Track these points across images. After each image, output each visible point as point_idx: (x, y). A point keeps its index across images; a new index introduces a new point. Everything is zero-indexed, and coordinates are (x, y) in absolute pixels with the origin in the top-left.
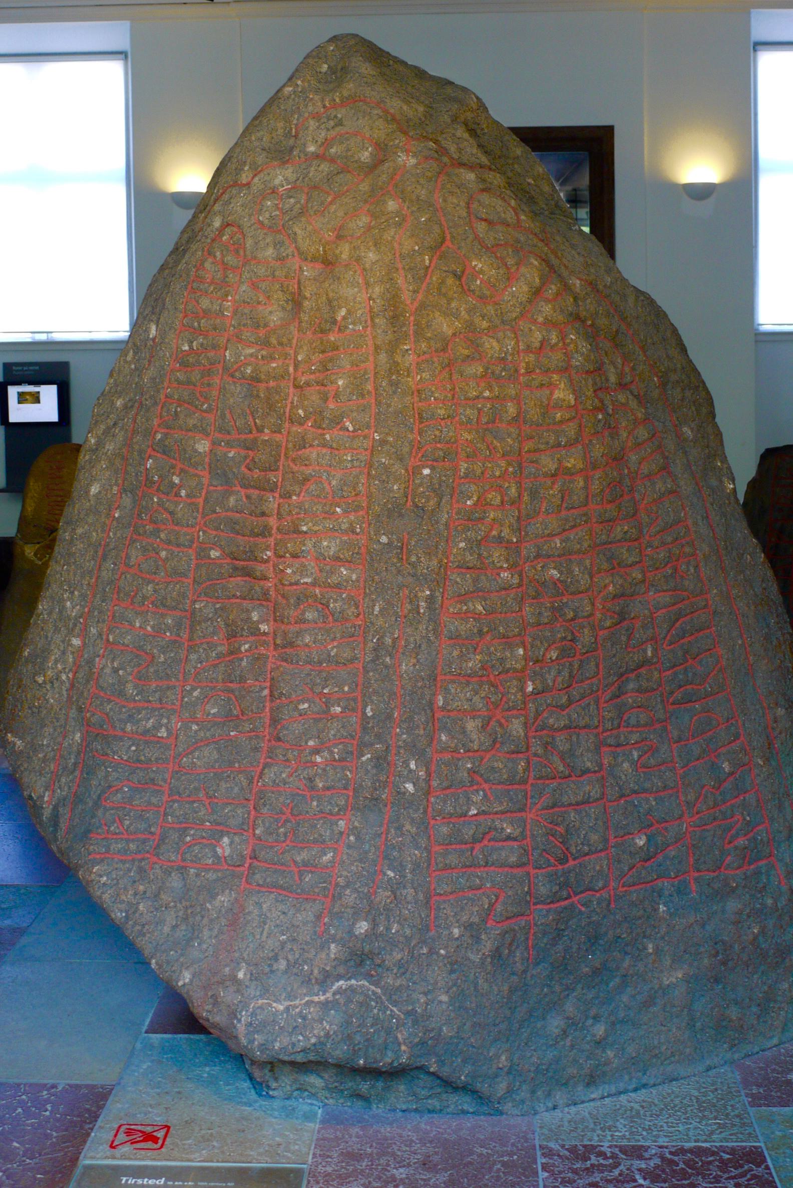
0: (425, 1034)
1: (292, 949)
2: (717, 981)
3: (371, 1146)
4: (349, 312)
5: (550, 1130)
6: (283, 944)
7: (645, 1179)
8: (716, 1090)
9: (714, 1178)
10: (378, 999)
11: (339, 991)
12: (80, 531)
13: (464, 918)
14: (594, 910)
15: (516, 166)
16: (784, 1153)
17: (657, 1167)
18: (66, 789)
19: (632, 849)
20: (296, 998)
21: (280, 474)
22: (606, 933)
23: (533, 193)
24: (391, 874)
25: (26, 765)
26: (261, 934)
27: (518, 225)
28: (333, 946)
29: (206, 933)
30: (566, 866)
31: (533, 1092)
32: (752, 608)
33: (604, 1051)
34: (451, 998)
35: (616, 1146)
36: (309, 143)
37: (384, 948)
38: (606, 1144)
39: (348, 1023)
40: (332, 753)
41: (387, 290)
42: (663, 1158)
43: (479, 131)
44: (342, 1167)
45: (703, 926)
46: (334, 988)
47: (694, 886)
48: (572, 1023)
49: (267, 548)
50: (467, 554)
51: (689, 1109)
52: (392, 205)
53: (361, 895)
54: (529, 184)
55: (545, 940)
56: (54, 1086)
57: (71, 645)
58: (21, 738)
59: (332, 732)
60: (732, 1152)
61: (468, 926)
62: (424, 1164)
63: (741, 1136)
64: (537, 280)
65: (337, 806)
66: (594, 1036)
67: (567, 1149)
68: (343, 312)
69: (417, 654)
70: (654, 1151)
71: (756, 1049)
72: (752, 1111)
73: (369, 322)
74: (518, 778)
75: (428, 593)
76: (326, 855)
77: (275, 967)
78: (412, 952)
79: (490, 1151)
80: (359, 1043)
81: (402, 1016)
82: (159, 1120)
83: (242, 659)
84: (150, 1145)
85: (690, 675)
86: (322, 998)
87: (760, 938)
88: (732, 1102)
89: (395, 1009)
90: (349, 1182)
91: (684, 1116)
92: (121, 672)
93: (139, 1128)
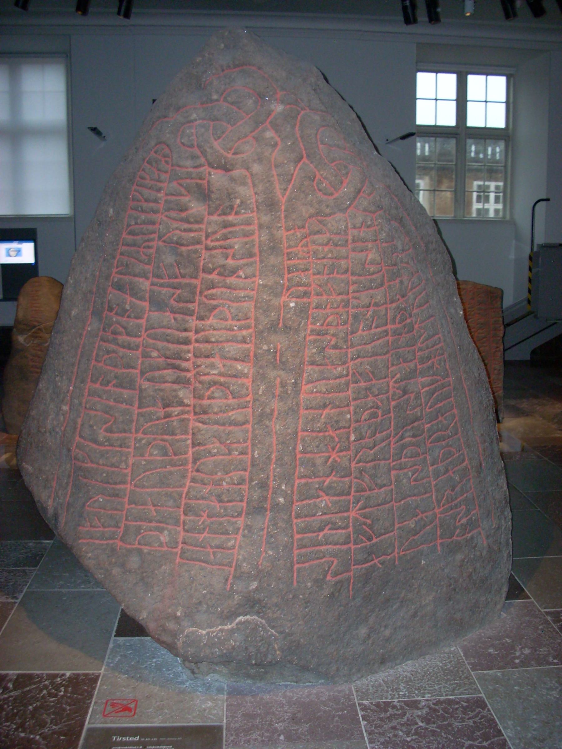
2: (450, 599)
4: (242, 202)
6: (204, 596)
7: (423, 722)
8: (451, 661)
9: (461, 719)
10: (263, 627)
11: (240, 623)
12: (65, 339)
16: (496, 700)
17: (427, 714)
18: (62, 498)
21: (196, 304)
24: (270, 553)
26: (191, 589)
35: (402, 701)
38: (396, 700)
40: (232, 479)
42: (430, 708)
44: (245, 724)
49: (189, 352)
51: (439, 674)
52: (269, 134)
55: (359, 585)
59: (233, 467)
60: (468, 701)
61: (316, 581)
62: (293, 719)
63: (471, 691)
65: (237, 512)
66: (385, 636)
67: (374, 705)
68: (238, 201)
70: (424, 703)
73: (255, 209)
74: (345, 492)
75: (294, 381)
77: (200, 609)
79: (330, 709)
81: (277, 635)
82: (131, 696)
84: (127, 713)
85: (440, 426)
86: (230, 627)
87: (473, 574)
89: (273, 631)
90: (251, 734)
93: (119, 702)
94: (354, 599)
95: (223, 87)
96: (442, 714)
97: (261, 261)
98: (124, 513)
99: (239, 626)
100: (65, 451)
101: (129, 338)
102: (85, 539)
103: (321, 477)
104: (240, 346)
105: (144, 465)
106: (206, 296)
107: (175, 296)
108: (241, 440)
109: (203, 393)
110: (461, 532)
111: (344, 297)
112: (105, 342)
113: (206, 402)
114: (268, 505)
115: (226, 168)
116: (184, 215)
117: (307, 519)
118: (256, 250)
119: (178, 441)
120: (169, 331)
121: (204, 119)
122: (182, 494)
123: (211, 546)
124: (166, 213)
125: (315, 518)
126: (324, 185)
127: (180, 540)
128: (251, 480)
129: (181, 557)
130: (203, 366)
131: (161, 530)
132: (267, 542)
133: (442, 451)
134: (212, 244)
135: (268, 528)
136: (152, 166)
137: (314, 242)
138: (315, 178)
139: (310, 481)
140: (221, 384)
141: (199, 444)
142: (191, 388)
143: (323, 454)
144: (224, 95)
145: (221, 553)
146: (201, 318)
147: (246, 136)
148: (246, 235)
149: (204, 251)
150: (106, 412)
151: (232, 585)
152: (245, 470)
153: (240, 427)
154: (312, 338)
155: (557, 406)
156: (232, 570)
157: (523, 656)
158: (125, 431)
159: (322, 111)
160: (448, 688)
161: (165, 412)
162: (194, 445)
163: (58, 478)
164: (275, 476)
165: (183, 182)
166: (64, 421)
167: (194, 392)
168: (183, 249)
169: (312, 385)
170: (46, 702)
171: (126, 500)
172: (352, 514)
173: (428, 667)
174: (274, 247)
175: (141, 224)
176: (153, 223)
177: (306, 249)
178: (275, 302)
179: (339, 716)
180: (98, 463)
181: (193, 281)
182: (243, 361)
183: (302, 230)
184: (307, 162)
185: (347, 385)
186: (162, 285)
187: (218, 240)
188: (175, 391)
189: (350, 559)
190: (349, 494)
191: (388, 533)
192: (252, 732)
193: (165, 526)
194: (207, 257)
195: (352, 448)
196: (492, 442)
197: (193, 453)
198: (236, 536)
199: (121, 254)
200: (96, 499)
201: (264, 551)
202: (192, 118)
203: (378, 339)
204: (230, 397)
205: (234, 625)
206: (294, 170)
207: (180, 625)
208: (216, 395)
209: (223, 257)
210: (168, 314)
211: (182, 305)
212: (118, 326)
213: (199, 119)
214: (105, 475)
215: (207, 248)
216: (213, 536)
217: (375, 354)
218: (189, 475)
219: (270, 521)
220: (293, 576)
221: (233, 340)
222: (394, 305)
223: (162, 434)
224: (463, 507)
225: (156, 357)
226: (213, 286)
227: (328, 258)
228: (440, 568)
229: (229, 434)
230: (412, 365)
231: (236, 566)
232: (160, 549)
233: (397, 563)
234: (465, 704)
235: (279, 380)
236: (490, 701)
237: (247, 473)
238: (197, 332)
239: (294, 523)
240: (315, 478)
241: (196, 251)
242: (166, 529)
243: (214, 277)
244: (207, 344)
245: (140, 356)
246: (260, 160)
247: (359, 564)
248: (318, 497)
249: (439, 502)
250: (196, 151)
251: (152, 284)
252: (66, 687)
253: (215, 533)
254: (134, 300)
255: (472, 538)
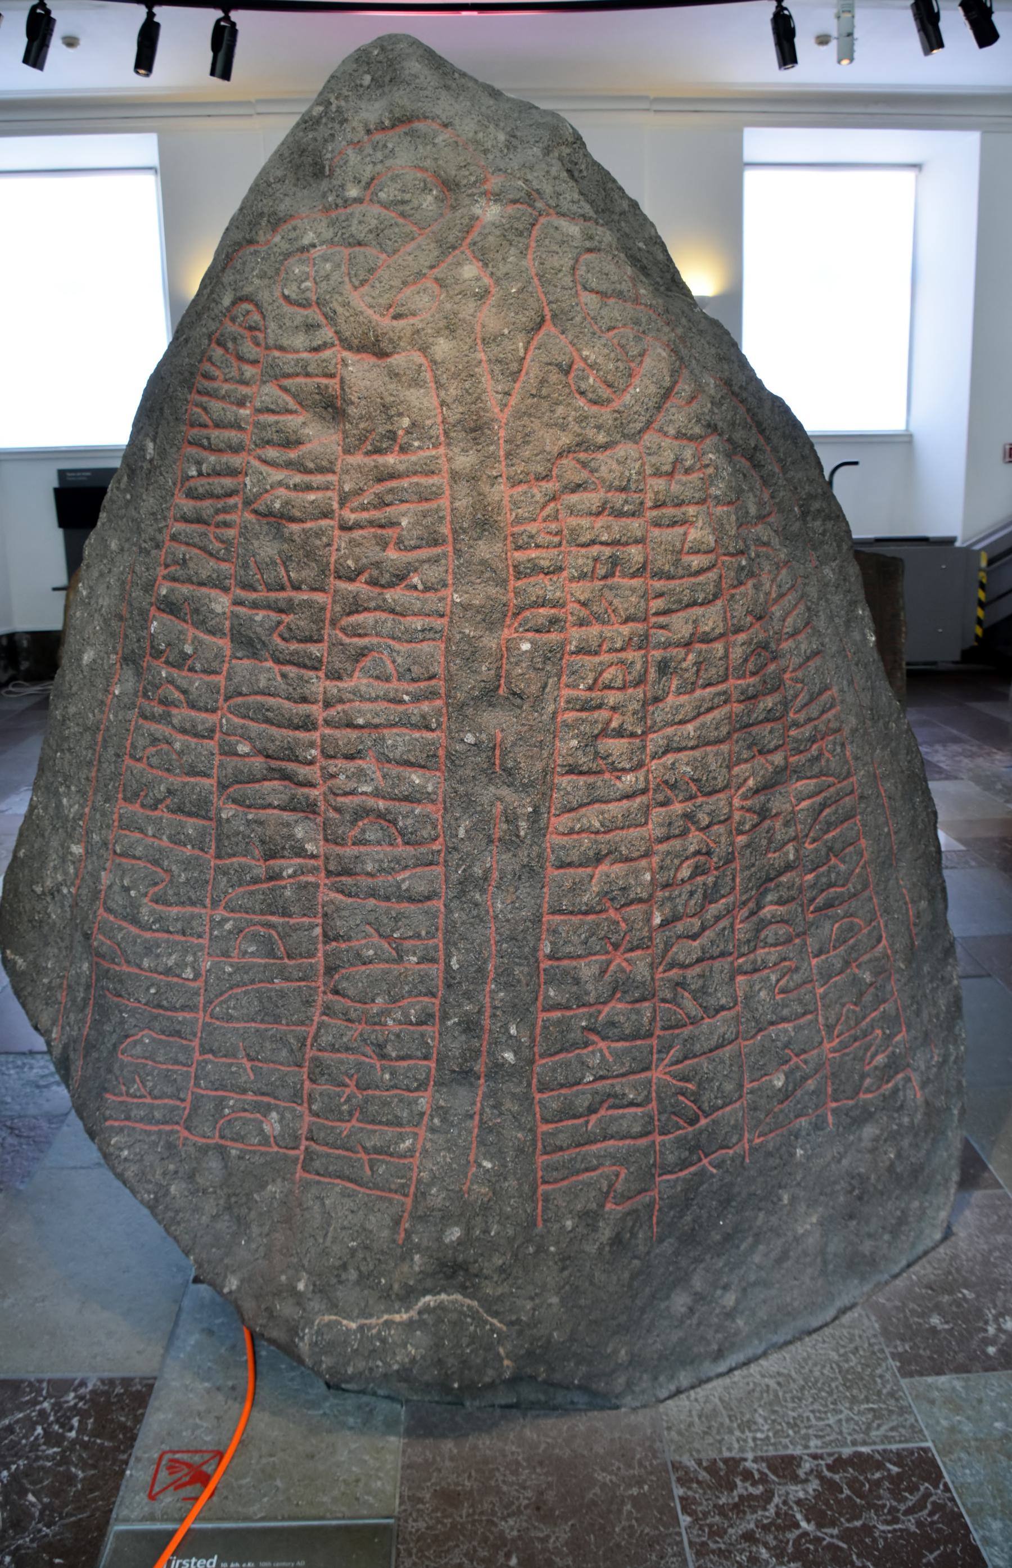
0: (532, 1344)
1: (365, 1259)
2: (851, 1217)
3: (470, 1477)
4: (413, 424)
5: (680, 1433)
6: (353, 1252)
7: (808, 1521)
8: (856, 1349)
10: (475, 1315)
11: (426, 1309)
12: (72, 710)
13: (579, 1207)
14: (727, 1171)
15: (623, 224)
16: (960, 1459)
17: (818, 1496)
19: (769, 1092)
20: (371, 1316)
22: (739, 1193)
23: (645, 261)
24: (488, 1165)
25: (29, 989)
26: (325, 1236)
27: (636, 300)
28: (417, 1257)
29: (255, 1230)
30: (697, 1126)
31: (655, 1378)
32: (900, 787)
33: (734, 1321)
34: (563, 1300)
36: (349, 185)
37: (482, 1255)
38: (750, 1456)
39: (438, 1346)
40: (406, 1015)
41: (467, 391)
43: (576, 174)
44: (439, 1521)
45: (839, 1161)
46: (420, 1304)
47: (830, 1119)
48: (699, 1298)
49: (312, 745)
50: (580, 753)
51: (833, 1385)
52: (470, 271)
53: (452, 1194)
54: (640, 249)
55: (672, 1213)
56: (83, 1383)
57: (71, 853)
58: (22, 955)
59: (407, 988)
63: (903, 1431)
64: (667, 378)
65: (416, 1080)
68: (406, 422)
69: (517, 889)
71: (886, 1276)
72: (904, 1382)
73: (442, 439)
75: (530, 809)
76: (404, 1142)
77: (344, 1277)
78: (515, 1256)
80: (453, 1365)
81: (504, 1328)
83: (285, 887)
86: (405, 1316)
88: (879, 1371)
89: (495, 1321)
90: (448, 1551)
91: (830, 1399)
92: (133, 893)
93: (184, 1457)
94: (661, 1240)
95: (369, 168)
96: (848, 1497)
97: (458, 553)
98: (192, 1070)
99: (425, 1316)
100: (78, 936)
101: (193, 713)
102: (116, 1120)
103: (591, 1005)
104: (417, 735)
105: (230, 974)
106: (343, 630)
107: (281, 627)
108: (423, 933)
109: (344, 833)
110: (871, 1085)
111: (639, 627)
112: (146, 718)
113: (350, 851)
114: (479, 1067)
115: (376, 347)
116: (293, 455)
117: (563, 1091)
118: (445, 530)
119: (295, 928)
120: (271, 701)
121: (331, 242)
122: (305, 1039)
123: (364, 1148)
124: (259, 452)
125: (580, 1087)
126: (591, 380)
127: (303, 1132)
128: (445, 1017)
129: (304, 1168)
130: (342, 777)
131: (265, 1110)
132: (482, 1143)
133: (837, 925)
134: (353, 517)
135: (481, 1114)
136: (227, 350)
137: (572, 511)
138: (570, 366)
139: (569, 1013)
140: (381, 815)
141: (336, 938)
142: (319, 820)
143: (594, 958)
144: (372, 189)
145: (387, 1163)
146: (336, 676)
147: (420, 275)
148: (424, 498)
149: (337, 532)
150: (156, 862)
151: (408, 1233)
152: (433, 995)
153: (420, 905)
154: (570, 716)
155: (998, 757)
156: (409, 1202)
157: (1003, 1337)
158: (193, 904)
159: (585, 218)
160: (857, 1424)
161: (268, 868)
162: (327, 938)
163: (69, 987)
164: (496, 1008)
165: (287, 382)
166: (76, 875)
167: (325, 830)
168: (295, 527)
169: (572, 815)
170: (38, 1458)
171: (196, 1043)
172: (657, 1074)
173: (810, 1363)
174: (484, 523)
175: (209, 475)
176: (233, 472)
177: (553, 526)
178: (490, 642)
179: (632, 1498)
180: (139, 966)
181: (319, 597)
182: (423, 767)
183: (543, 484)
184: (554, 331)
185: (646, 810)
186: (255, 605)
187: (364, 508)
188: (288, 825)
189: (654, 1165)
190: (649, 1035)
191: (731, 1103)
192: (451, 1544)
193: (273, 1101)
194: (343, 545)
195: (658, 939)
196: (933, 897)
197: (326, 955)
198: (416, 1130)
199: (174, 538)
200: (138, 1037)
201: (475, 1162)
202: (306, 241)
203: (709, 710)
204: (399, 840)
205: (413, 1313)
206: (526, 350)
207: (304, 1310)
208: (370, 836)
209: (378, 544)
210: (269, 664)
211: (294, 646)
212: (171, 687)
213: (322, 243)
214: (153, 991)
215: (345, 528)
216: (369, 1127)
217: (703, 742)
218: (320, 999)
219: (486, 1096)
220: (535, 1209)
221: (404, 722)
222: (742, 637)
223: (262, 913)
224: (878, 1032)
225: (247, 755)
226: (356, 607)
227: (602, 543)
228: (834, 1157)
229: (396, 920)
230: (778, 758)
231: (415, 1195)
232: (263, 1149)
233: (747, 1160)
234: (895, 1469)
235: (499, 807)
236: (946, 1460)
237: (437, 1002)
238: (327, 705)
239: (536, 1101)
240: (578, 1007)
241: (319, 534)
242: (276, 1108)
243: (359, 587)
244: (349, 730)
245: (216, 751)
246: (451, 328)
247: (671, 1172)
248: (586, 1044)
249: (830, 1028)
250: (314, 314)
251: (238, 602)
252: (84, 1415)
253: (373, 1122)
254: (202, 636)
255: (895, 1091)
